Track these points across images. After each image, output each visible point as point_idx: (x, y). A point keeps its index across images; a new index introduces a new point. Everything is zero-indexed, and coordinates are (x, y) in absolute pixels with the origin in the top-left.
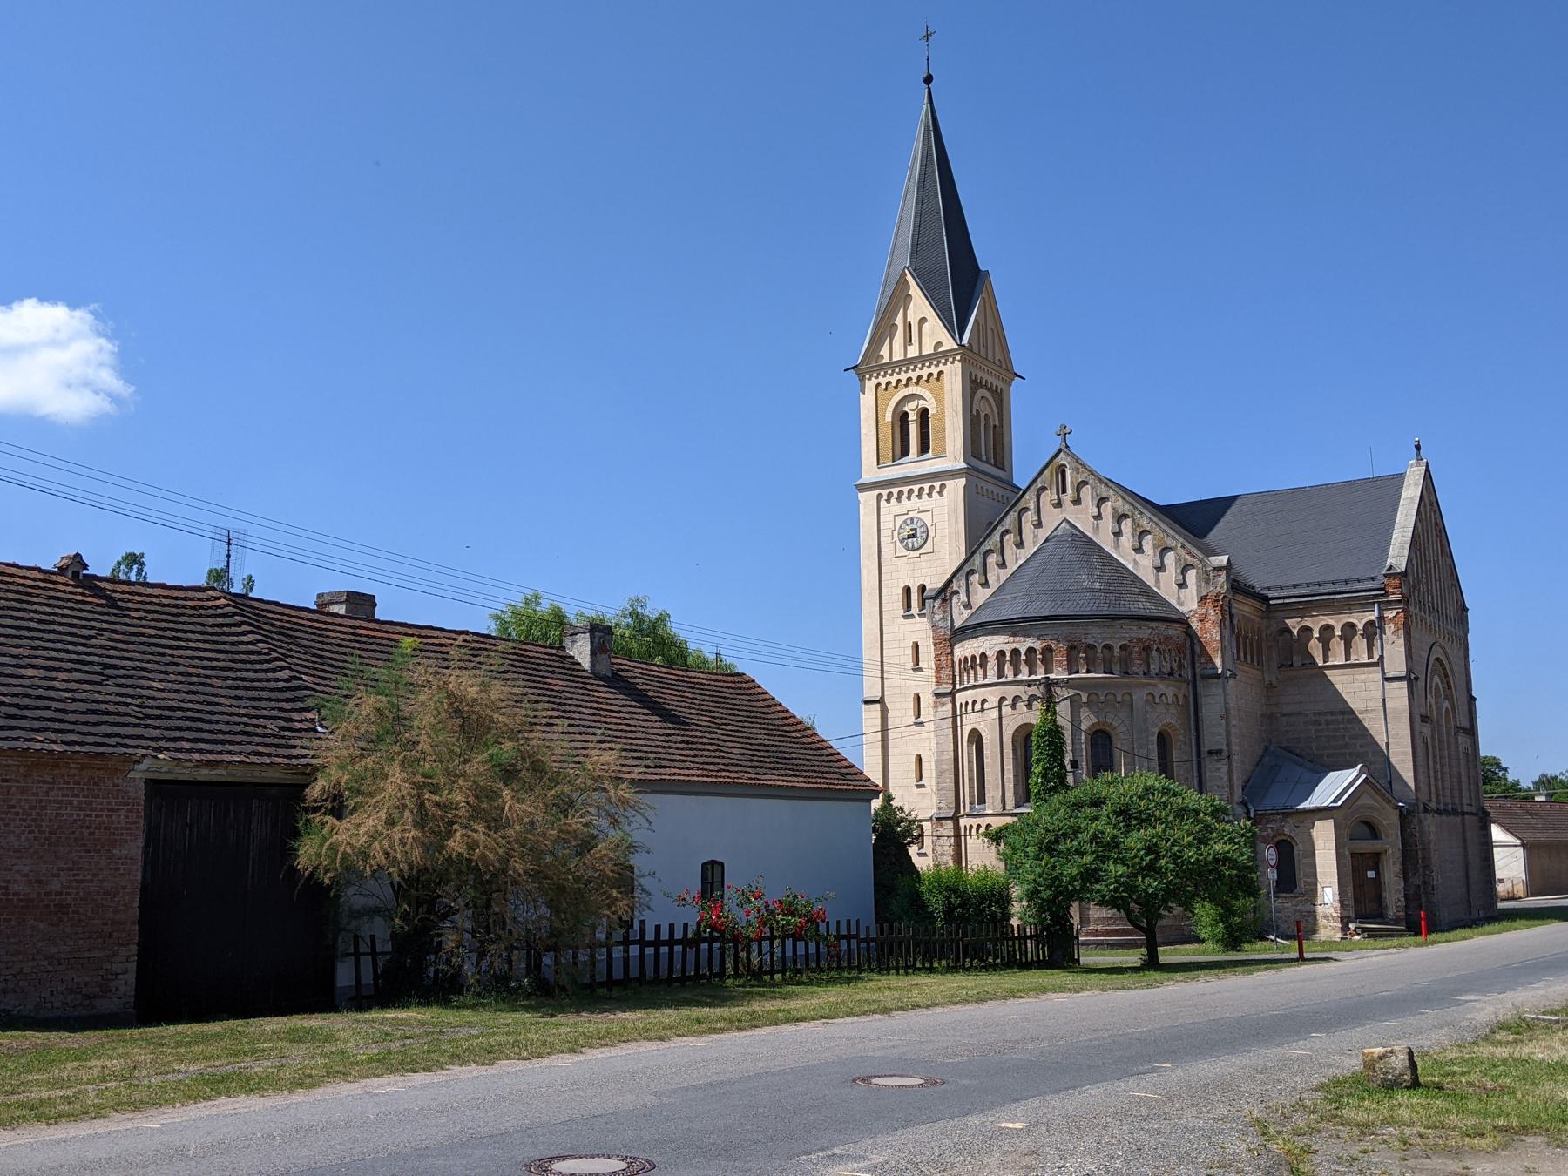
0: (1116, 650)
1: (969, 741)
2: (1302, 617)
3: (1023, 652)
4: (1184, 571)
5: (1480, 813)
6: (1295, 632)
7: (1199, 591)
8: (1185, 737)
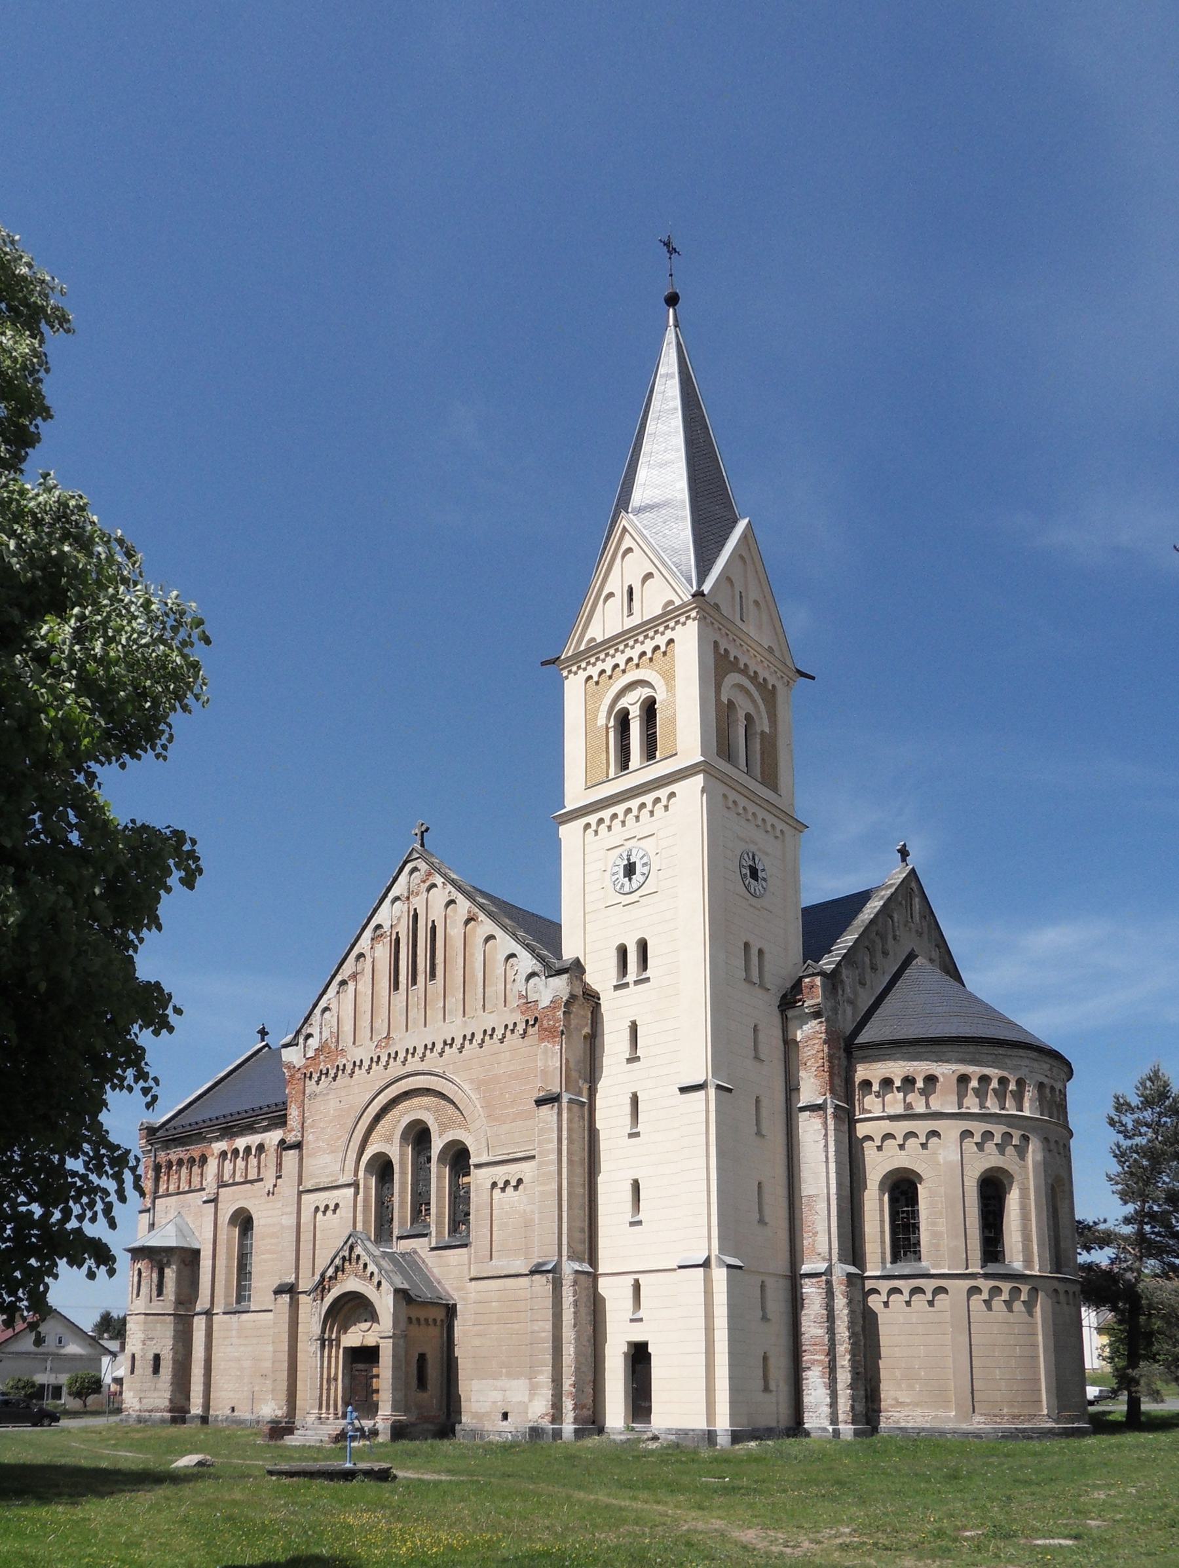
1: (441, 1159)
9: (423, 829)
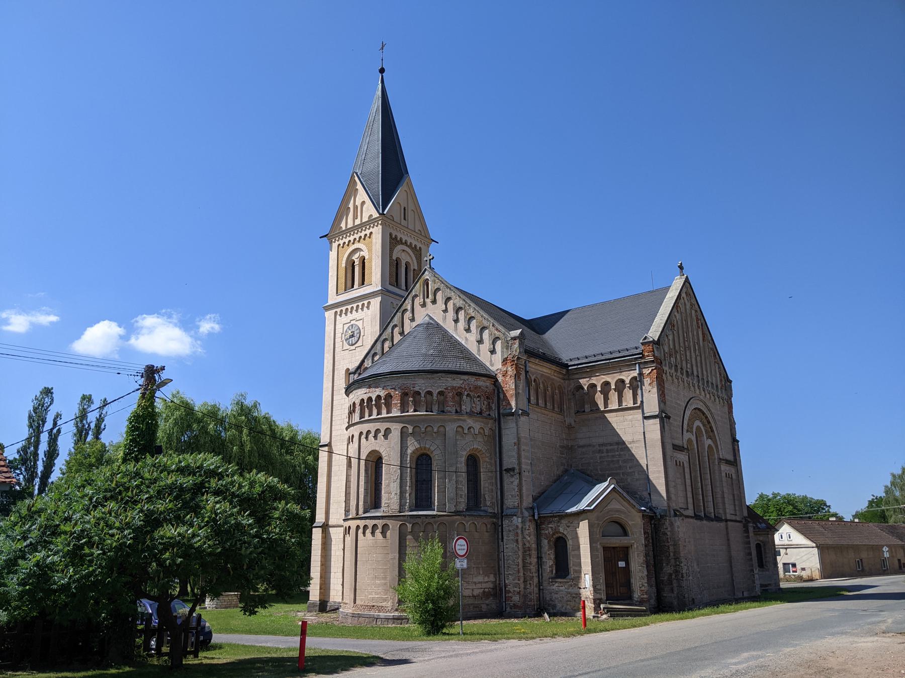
0: (435, 395)
2: (590, 377)
3: (374, 399)
4: (494, 343)
5: (744, 521)
6: (586, 388)
7: (502, 355)
8: (491, 459)
9: (431, 257)
